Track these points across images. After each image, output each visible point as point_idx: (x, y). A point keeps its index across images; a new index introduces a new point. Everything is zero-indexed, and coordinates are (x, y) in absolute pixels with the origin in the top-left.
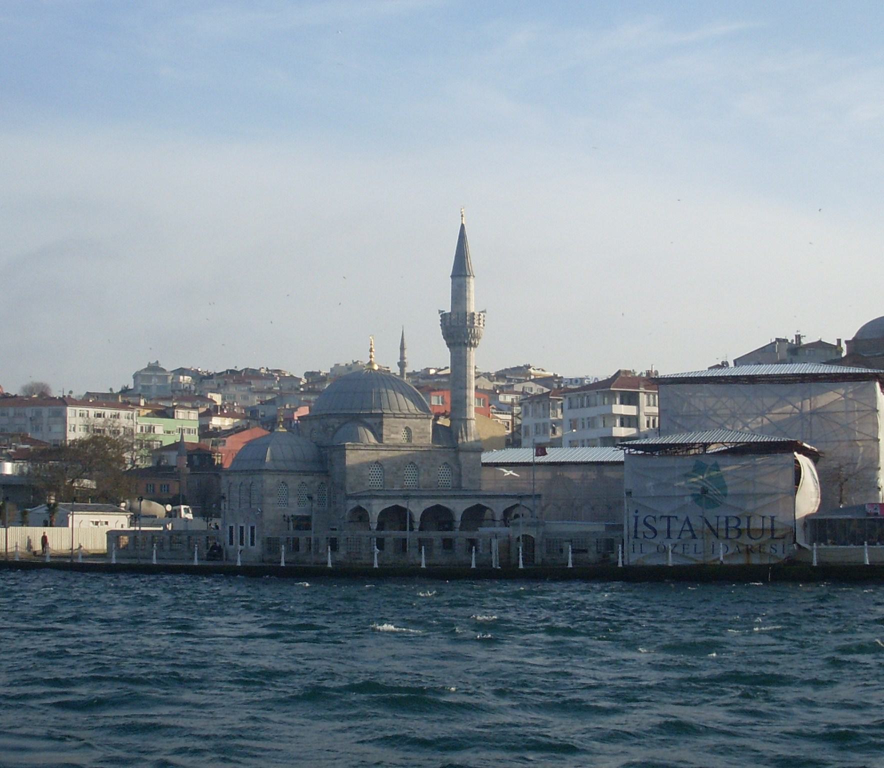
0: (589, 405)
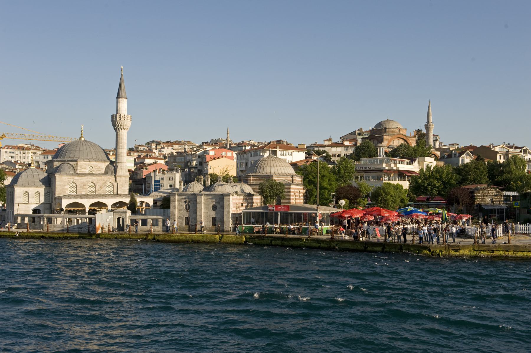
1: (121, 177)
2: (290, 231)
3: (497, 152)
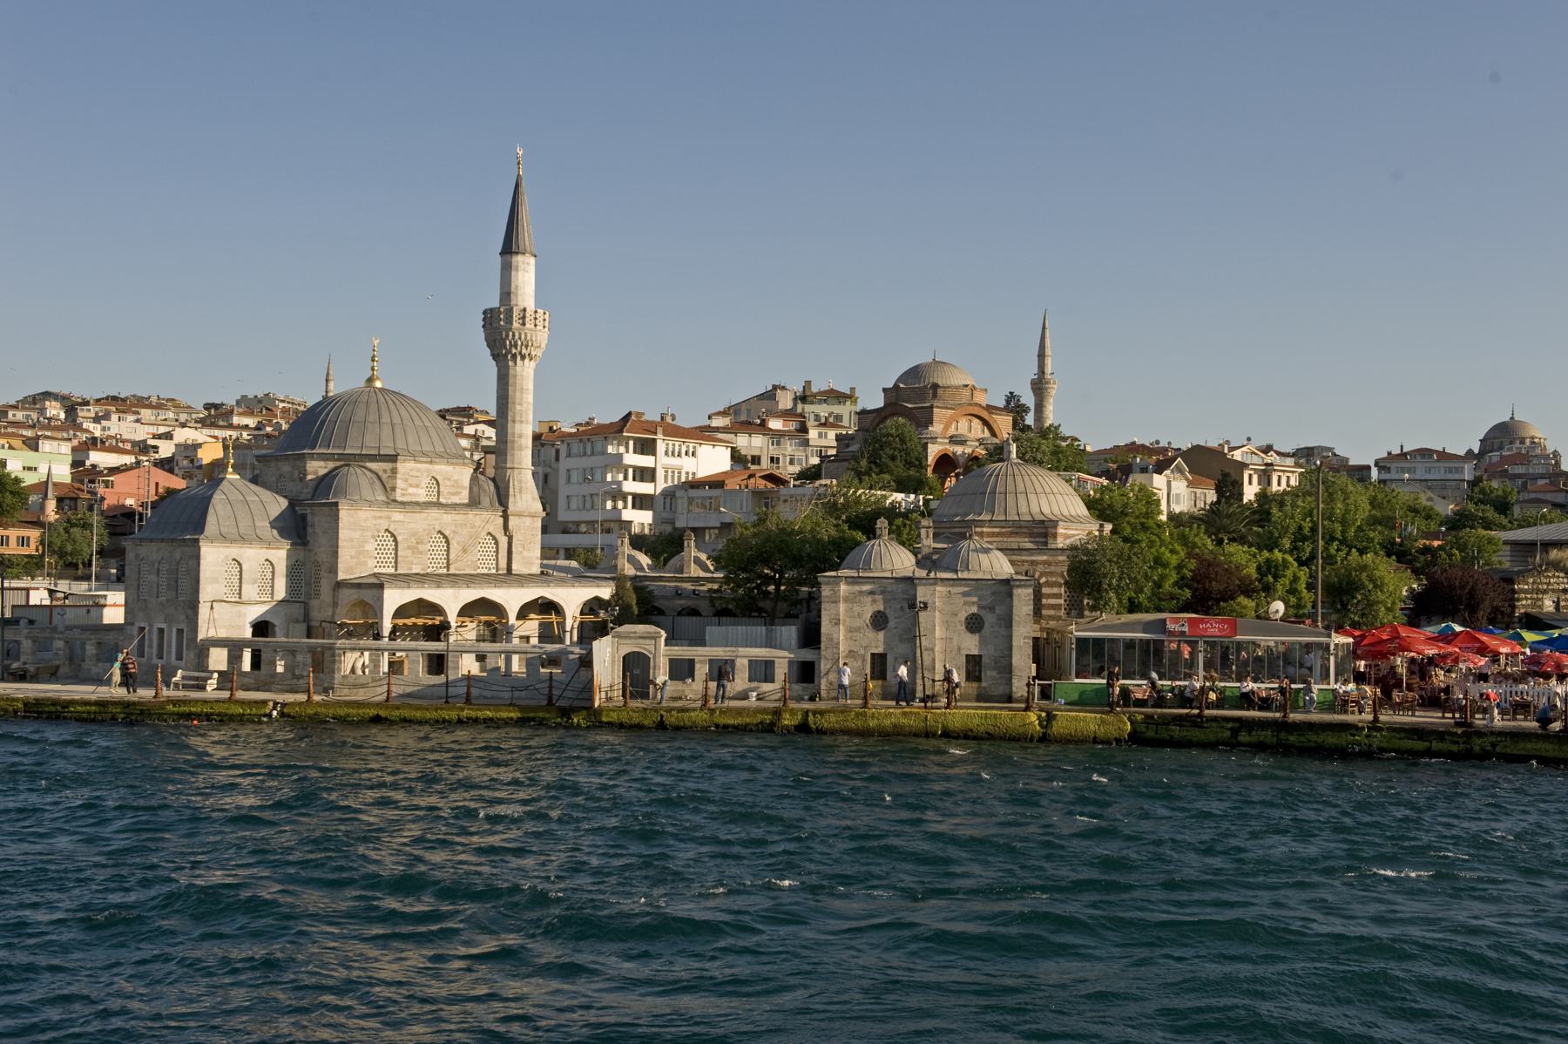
0: (593, 454)
1: (520, 515)
2: (1246, 700)
3: (1244, 466)
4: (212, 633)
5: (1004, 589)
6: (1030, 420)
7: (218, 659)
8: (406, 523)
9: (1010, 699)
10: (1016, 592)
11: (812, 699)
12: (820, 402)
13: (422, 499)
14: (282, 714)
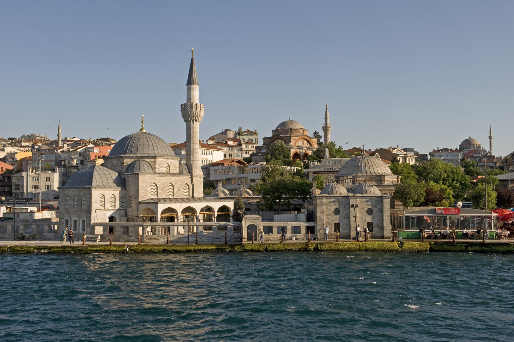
2: (466, 236)
4: (96, 221)
5: (380, 199)
6: (322, 140)
7: (99, 230)
8: (161, 181)
9: (383, 237)
10: (384, 200)
11: (315, 239)
12: (245, 135)
13: (165, 172)
14: (130, 249)
